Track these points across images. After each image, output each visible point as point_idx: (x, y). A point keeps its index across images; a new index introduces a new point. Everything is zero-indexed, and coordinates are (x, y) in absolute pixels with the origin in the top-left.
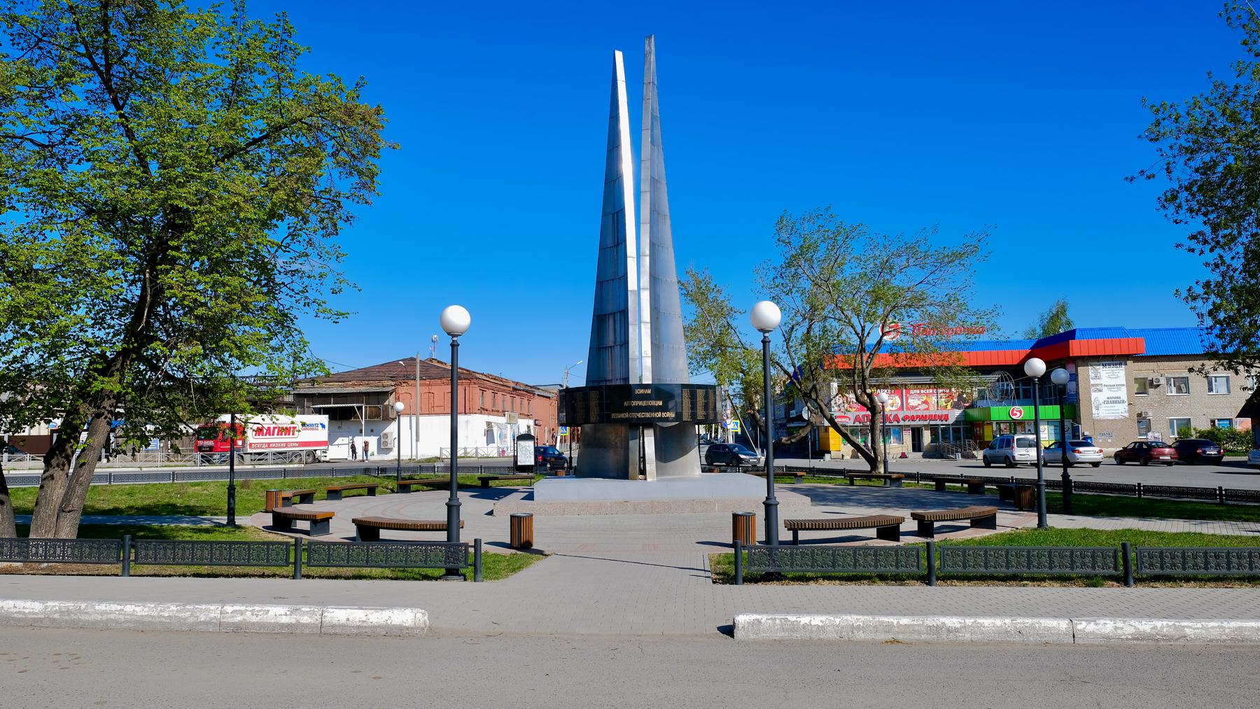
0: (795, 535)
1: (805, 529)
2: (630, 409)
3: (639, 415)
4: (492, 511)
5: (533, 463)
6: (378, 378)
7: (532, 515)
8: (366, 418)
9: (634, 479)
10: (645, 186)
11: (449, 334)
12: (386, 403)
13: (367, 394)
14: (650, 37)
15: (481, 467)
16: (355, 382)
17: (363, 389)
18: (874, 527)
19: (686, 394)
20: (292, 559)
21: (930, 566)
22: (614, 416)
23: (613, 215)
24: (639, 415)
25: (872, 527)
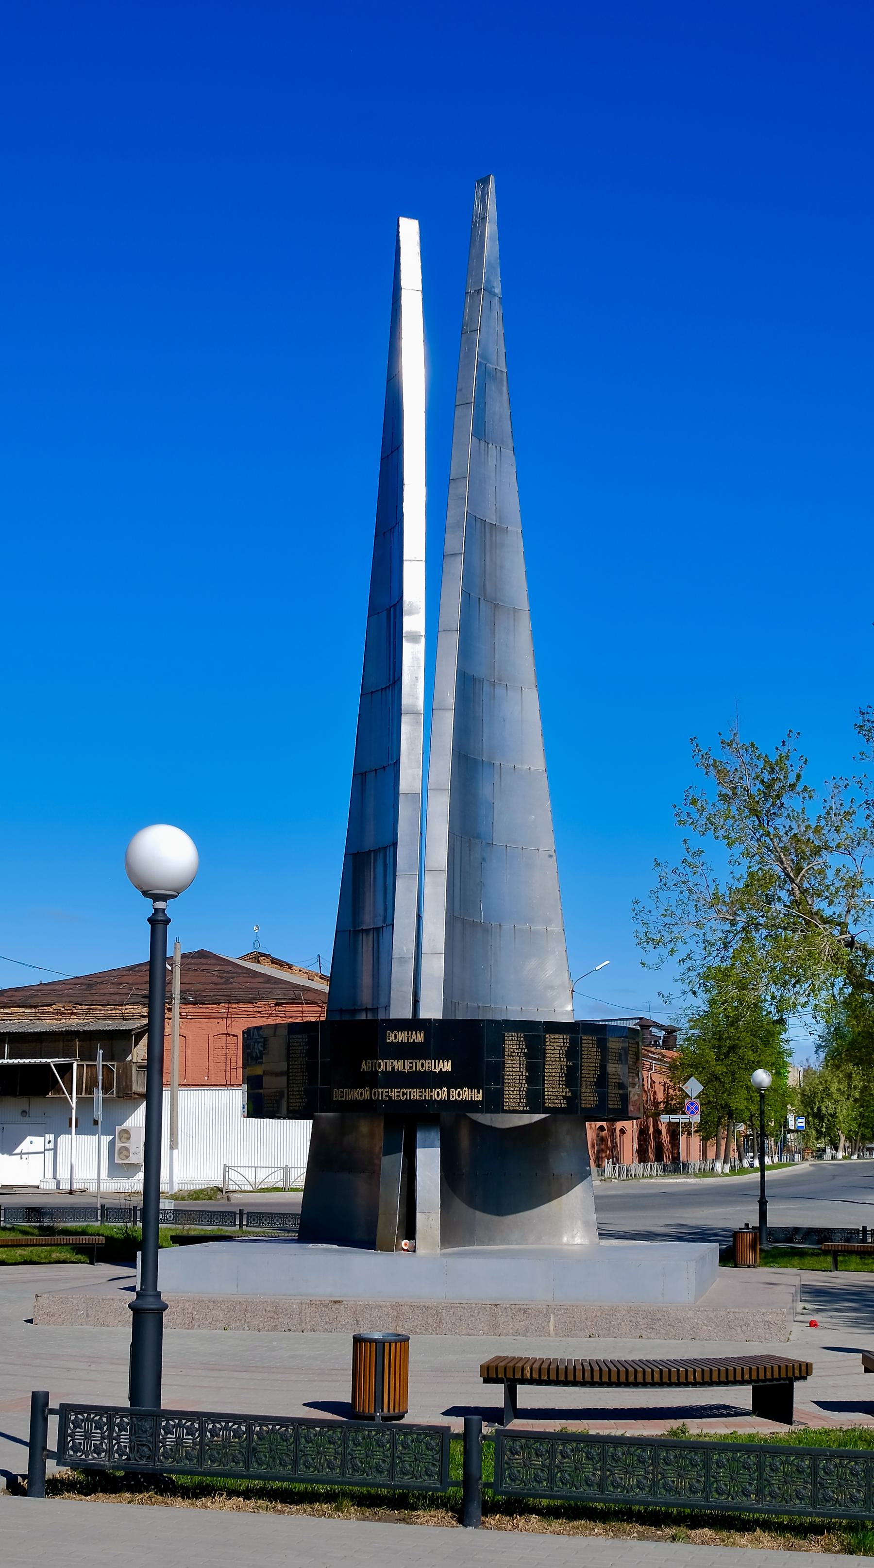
0: (511, 1395)
1: (531, 1382)
2: (372, 1080)
3: (394, 1094)
4: (32, 1319)
5: (768, 1226)
6: (112, 999)
7: (404, 1340)
8: (79, 1092)
9: (389, 1247)
10: (455, 541)
11: (145, 893)
12: (129, 1059)
13: (70, 1035)
14: (485, 181)
15: (241, 1212)
16: (59, 1007)
17: (74, 1023)
18: (748, 1382)
19: (513, 1045)
20: (53, 1422)
21: (468, 1482)
22: (338, 1094)
23: (389, 610)
24: (394, 1094)
25: (742, 1382)
